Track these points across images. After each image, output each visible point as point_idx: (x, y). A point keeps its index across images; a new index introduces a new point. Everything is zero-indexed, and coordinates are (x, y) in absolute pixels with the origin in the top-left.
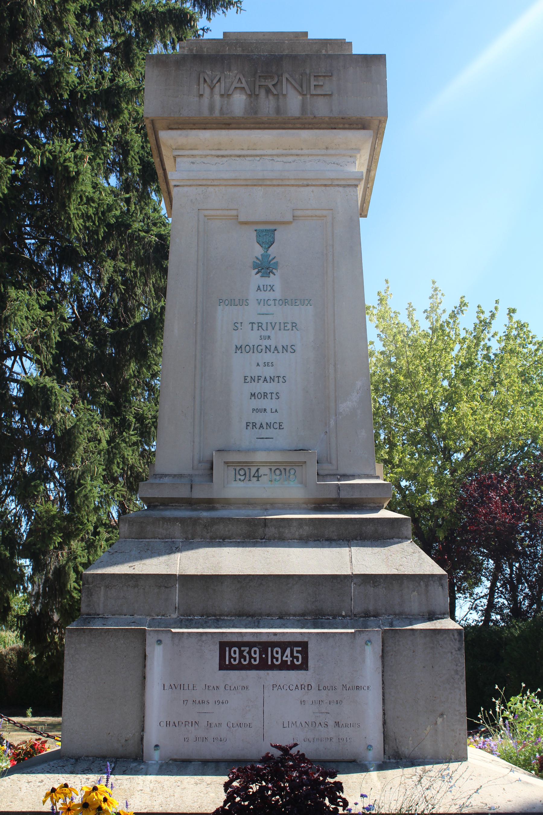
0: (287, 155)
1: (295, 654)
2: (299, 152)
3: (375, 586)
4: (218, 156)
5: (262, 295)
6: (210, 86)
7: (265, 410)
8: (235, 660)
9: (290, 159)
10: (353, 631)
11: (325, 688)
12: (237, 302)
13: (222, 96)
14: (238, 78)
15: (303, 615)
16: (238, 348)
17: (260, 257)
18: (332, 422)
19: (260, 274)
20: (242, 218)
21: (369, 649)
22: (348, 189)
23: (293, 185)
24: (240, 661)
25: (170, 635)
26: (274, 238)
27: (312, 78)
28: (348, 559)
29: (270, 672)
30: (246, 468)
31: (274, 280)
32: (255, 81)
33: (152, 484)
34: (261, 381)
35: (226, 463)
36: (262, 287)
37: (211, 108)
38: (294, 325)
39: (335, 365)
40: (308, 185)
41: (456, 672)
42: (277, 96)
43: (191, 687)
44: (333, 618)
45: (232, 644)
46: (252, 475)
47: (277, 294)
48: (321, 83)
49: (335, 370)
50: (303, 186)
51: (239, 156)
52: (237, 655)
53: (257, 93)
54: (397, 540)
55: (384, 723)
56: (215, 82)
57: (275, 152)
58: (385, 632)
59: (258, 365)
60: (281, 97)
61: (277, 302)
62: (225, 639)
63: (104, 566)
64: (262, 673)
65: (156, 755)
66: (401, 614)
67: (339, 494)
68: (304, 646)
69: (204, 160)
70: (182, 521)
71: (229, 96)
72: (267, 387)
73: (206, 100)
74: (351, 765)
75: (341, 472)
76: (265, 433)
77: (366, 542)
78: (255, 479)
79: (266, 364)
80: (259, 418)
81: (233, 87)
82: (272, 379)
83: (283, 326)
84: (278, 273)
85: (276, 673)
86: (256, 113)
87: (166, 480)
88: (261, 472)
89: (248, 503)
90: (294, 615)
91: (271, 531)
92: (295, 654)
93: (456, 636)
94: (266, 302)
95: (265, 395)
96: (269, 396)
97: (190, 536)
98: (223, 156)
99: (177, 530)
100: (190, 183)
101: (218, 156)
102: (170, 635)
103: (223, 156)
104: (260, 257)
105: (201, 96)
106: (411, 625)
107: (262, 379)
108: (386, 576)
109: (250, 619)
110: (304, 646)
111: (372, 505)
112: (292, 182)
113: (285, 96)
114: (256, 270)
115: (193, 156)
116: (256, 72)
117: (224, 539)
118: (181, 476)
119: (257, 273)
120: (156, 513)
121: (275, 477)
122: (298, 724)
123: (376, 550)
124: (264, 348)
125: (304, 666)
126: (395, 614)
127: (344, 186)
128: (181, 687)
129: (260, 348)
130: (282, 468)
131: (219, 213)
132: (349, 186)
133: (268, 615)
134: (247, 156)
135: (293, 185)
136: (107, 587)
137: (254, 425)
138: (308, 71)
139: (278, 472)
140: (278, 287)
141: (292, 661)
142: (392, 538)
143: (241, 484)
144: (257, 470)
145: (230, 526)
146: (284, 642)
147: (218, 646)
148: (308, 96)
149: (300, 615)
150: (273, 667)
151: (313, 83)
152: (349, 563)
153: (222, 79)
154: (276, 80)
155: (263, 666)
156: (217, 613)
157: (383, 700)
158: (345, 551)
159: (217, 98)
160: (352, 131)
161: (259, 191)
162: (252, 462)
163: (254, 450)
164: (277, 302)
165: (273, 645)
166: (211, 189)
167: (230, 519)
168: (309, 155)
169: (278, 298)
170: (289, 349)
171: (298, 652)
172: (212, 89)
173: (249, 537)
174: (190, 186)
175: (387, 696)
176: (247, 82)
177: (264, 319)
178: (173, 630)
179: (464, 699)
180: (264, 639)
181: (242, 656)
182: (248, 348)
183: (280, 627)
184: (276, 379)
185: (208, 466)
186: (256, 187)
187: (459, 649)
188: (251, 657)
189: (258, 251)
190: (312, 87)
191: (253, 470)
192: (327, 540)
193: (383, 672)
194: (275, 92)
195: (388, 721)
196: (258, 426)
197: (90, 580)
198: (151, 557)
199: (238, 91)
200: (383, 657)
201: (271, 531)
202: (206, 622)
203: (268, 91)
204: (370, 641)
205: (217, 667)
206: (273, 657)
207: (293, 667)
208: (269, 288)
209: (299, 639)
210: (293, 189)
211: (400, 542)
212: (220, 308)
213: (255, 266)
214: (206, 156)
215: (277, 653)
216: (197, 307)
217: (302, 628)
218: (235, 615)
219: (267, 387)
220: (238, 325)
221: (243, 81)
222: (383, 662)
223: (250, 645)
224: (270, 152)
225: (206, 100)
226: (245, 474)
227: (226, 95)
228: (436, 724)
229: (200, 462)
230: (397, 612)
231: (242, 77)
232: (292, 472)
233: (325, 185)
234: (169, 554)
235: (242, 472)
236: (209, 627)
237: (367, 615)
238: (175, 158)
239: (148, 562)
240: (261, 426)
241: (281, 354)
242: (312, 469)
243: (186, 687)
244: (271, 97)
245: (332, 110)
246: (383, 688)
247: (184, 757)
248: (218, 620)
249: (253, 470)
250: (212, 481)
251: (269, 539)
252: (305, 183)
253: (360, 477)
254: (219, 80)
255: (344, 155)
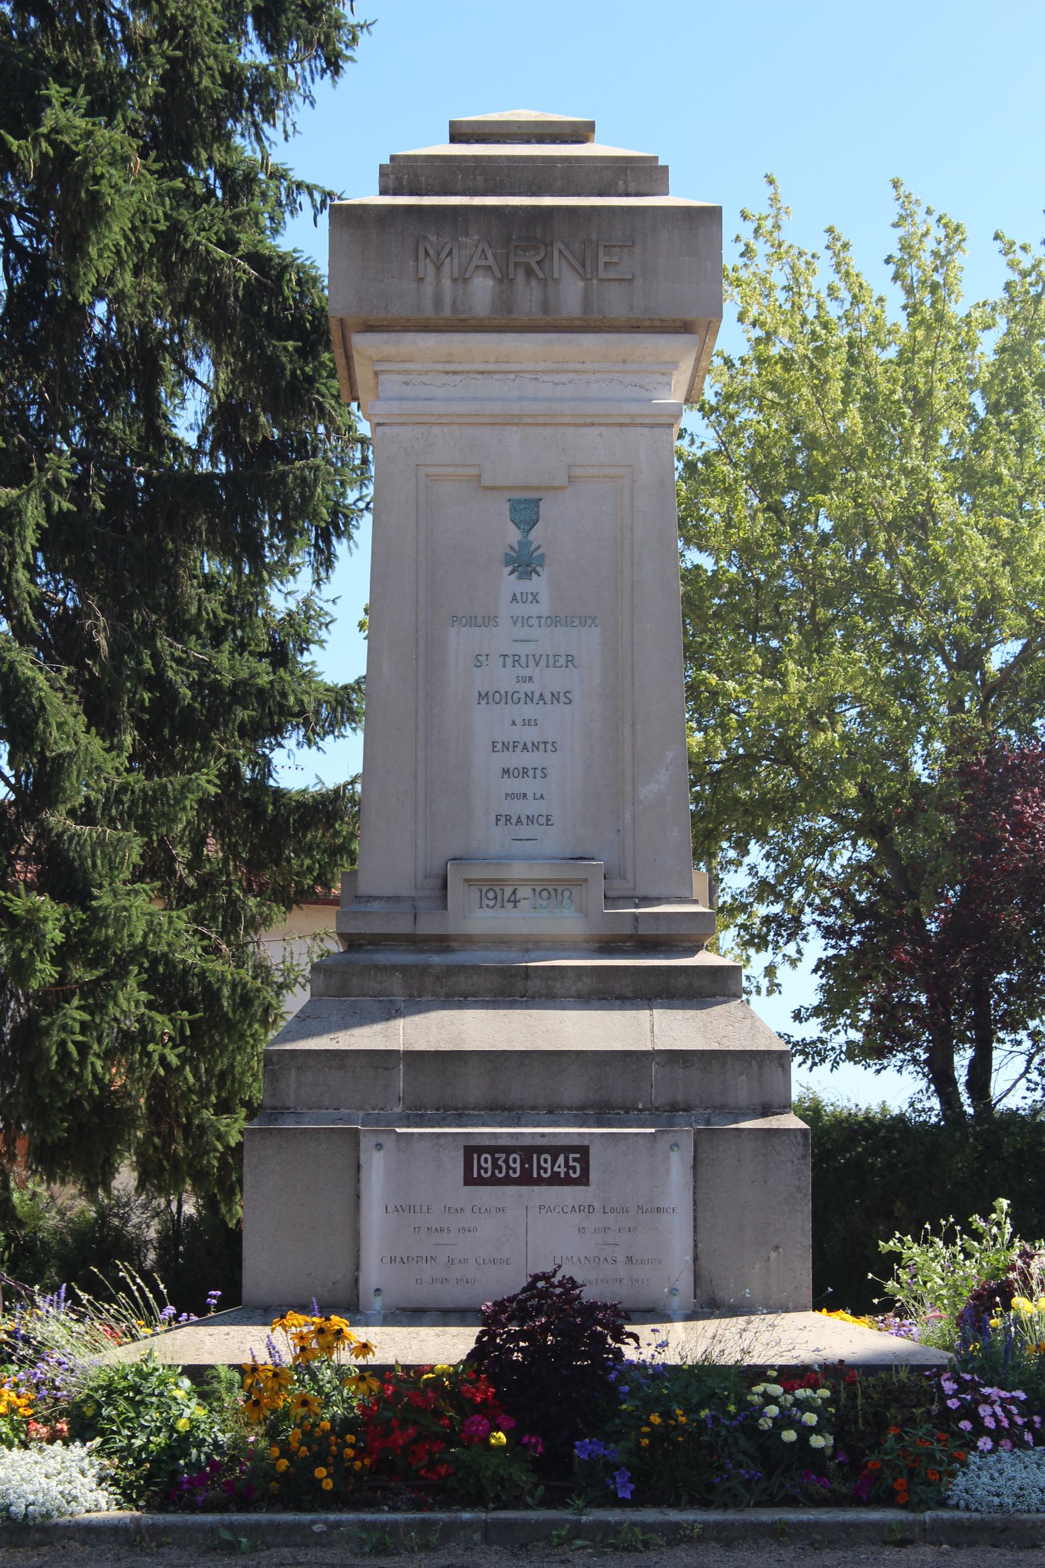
0: (558, 372)
1: (571, 1163)
2: (579, 367)
3: (685, 1068)
4: (446, 373)
5: (520, 609)
6: (434, 263)
7: (525, 795)
8: (486, 1171)
9: (564, 378)
10: (653, 1130)
11: (613, 1210)
12: (480, 621)
13: (454, 280)
14: (480, 249)
15: (582, 1108)
16: (483, 696)
17: (516, 547)
18: (628, 816)
19: (516, 574)
20: (487, 481)
21: (675, 1157)
22: (657, 431)
23: (569, 425)
24: (493, 1173)
25: (394, 1137)
26: (537, 514)
27: (601, 253)
28: (648, 1026)
29: (535, 1188)
30: (497, 889)
31: (538, 584)
32: (508, 254)
33: (356, 913)
34: (518, 750)
35: (467, 881)
36: (519, 597)
37: (438, 302)
38: (570, 659)
39: (633, 726)
40: (593, 424)
41: (799, 1189)
42: (544, 282)
43: (425, 1209)
44: (626, 1112)
45: (481, 1150)
46: (506, 898)
47: (543, 608)
48: (615, 260)
49: (634, 734)
50: (585, 425)
51: (482, 373)
52: (489, 1165)
53: (512, 276)
54: (721, 999)
55: (696, 1259)
56: (443, 255)
57: (541, 366)
58: (698, 1132)
59: (514, 723)
60: (550, 282)
61: (543, 621)
62: (472, 1143)
63: (294, 1039)
64: (524, 1189)
65: (377, 1303)
66: (722, 1107)
67: (636, 928)
68: (583, 1152)
69: (423, 378)
70: (404, 969)
71: (466, 281)
72: (528, 759)
73: (429, 288)
74: (648, 1315)
75: (642, 892)
76: (524, 831)
77: (676, 1002)
78: (511, 905)
79: (526, 723)
80: (516, 808)
81: (472, 266)
82: (535, 746)
83: (553, 660)
84: (544, 572)
85: (544, 1189)
86: (510, 310)
87: (376, 906)
88: (520, 894)
89: (501, 942)
90: (570, 1108)
91: (535, 985)
92: (571, 1163)
93: (799, 1139)
94: (525, 621)
95: (525, 772)
96: (531, 773)
97: (415, 993)
98: (455, 373)
99: (396, 983)
100: (404, 419)
101: (446, 373)
102: (394, 1137)
103: (455, 373)
104: (516, 547)
105: (420, 280)
106: (737, 1122)
107: (521, 746)
108: (703, 1053)
109: (506, 1113)
110: (583, 1152)
111: (686, 944)
112: (567, 420)
113: (557, 281)
114: (510, 568)
115: (407, 372)
116: (509, 240)
117: (466, 997)
118: (396, 899)
119: (511, 573)
120: (361, 958)
121: (540, 902)
122: (575, 1260)
123: (690, 1013)
124: (523, 696)
125: (584, 1180)
126: (715, 1108)
127: (652, 426)
128: (412, 1209)
129: (516, 696)
130: (551, 888)
131: (450, 470)
132: (659, 425)
133: (533, 1108)
134: (495, 372)
135: (569, 425)
136: (299, 1068)
137: (508, 819)
138: (594, 237)
139: (545, 894)
140: (544, 596)
141: (567, 1174)
142: (714, 996)
143: (490, 912)
144: (514, 892)
145: (475, 978)
146: (555, 1147)
147: (462, 1152)
148: (595, 282)
149: (577, 1108)
150: (540, 1181)
151: (603, 259)
152: (649, 1034)
153: (455, 250)
154: (542, 254)
155: (526, 1179)
156: (460, 1105)
157: (695, 1227)
158: (643, 1015)
159: (447, 283)
160: (666, 336)
161: (514, 435)
162: (506, 880)
163: (510, 858)
164: (543, 621)
165: (540, 1150)
166: (436, 430)
167: (475, 968)
168: (594, 372)
169: (545, 615)
170: (562, 699)
171: (575, 1160)
172: (438, 268)
173: (503, 994)
174: (403, 424)
175: (700, 1221)
176: (494, 256)
177: (523, 650)
178: (398, 1130)
179: (809, 1226)
180: (527, 1142)
181: (496, 1166)
182: (497, 696)
183: (550, 1126)
184: (542, 746)
185: (439, 883)
186: (509, 428)
187: (804, 1157)
188: (508, 1167)
189: (513, 535)
190: (601, 266)
191: (508, 892)
192: (618, 998)
193: (695, 1188)
194: (541, 276)
195: (701, 1256)
196: (514, 820)
197: (275, 1059)
198: (361, 1024)
199: (481, 272)
200: (695, 1167)
201: (535, 985)
202: (444, 1119)
203: (530, 273)
204: (676, 1145)
205: (462, 1181)
206: (539, 1167)
207: (568, 1181)
208: (530, 598)
209: (576, 1142)
210: (569, 430)
211: (726, 1002)
212: (453, 631)
213: (508, 561)
214: (427, 373)
215: (546, 1161)
216: (417, 630)
217: (581, 1126)
218: (485, 1108)
219: (528, 759)
220: (483, 659)
221: (490, 255)
222: (695, 1174)
223: (508, 1150)
224: (531, 366)
225: (429, 288)
226: (496, 898)
227: (462, 279)
228: (768, 1260)
229: (426, 877)
230: (717, 1104)
231: (487, 248)
232: (567, 894)
233: (621, 425)
234: (387, 1019)
235: (491, 895)
236: (449, 1126)
237: (674, 1108)
238: (376, 374)
239: (357, 1031)
240: (519, 821)
241: (549, 705)
242: (597, 889)
243: (418, 1209)
244: (534, 283)
245: (631, 308)
246: (695, 1211)
247: (415, 1305)
248: (460, 1115)
249: (508, 892)
250: (445, 908)
251: (533, 997)
252: (589, 420)
253: (668, 900)
254: (450, 253)
255: (652, 372)
